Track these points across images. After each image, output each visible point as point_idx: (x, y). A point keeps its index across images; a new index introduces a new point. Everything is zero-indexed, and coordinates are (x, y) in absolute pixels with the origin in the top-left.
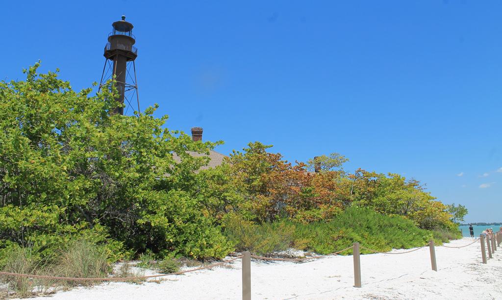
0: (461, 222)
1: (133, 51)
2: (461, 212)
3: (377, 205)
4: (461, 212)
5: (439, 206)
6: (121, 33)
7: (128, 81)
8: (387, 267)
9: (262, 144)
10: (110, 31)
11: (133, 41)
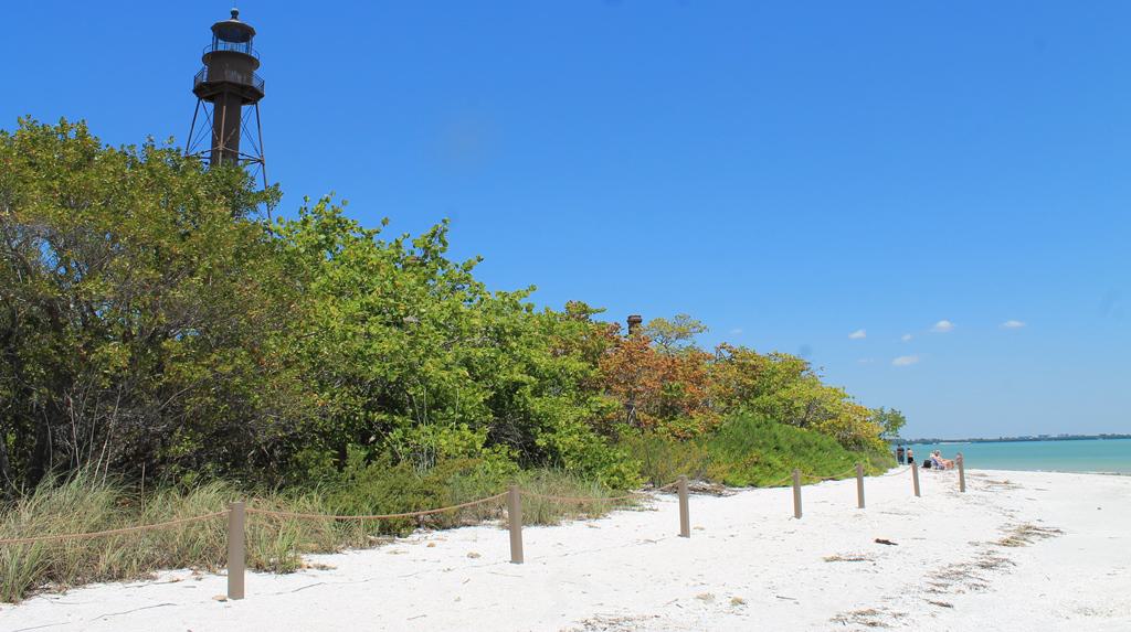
1: (255, 84)
2: (895, 421)
4: (895, 421)
5: (859, 411)
7: (245, 147)
9: (591, 307)
10: (206, 42)
11: (252, 62)
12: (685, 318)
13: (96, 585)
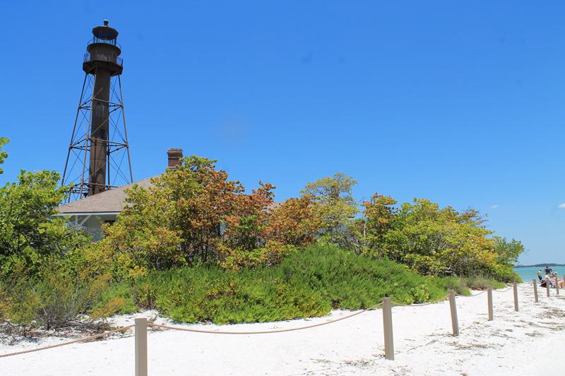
0: (516, 264)
1: (119, 63)
3: (389, 242)
4: (516, 249)
6: (101, 41)
7: (113, 99)
8: (419, 321)
10: (90, 39)
11: (118, 51)
12: (339, 176)
13: (336, 314)
